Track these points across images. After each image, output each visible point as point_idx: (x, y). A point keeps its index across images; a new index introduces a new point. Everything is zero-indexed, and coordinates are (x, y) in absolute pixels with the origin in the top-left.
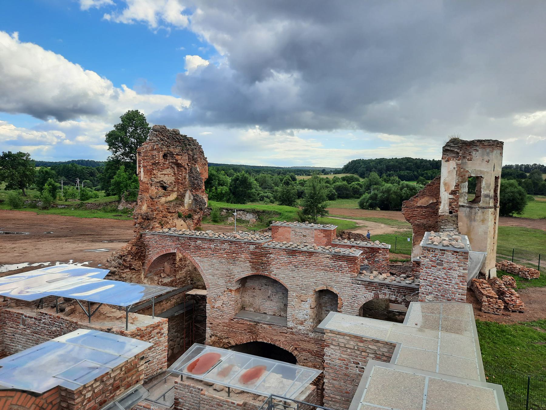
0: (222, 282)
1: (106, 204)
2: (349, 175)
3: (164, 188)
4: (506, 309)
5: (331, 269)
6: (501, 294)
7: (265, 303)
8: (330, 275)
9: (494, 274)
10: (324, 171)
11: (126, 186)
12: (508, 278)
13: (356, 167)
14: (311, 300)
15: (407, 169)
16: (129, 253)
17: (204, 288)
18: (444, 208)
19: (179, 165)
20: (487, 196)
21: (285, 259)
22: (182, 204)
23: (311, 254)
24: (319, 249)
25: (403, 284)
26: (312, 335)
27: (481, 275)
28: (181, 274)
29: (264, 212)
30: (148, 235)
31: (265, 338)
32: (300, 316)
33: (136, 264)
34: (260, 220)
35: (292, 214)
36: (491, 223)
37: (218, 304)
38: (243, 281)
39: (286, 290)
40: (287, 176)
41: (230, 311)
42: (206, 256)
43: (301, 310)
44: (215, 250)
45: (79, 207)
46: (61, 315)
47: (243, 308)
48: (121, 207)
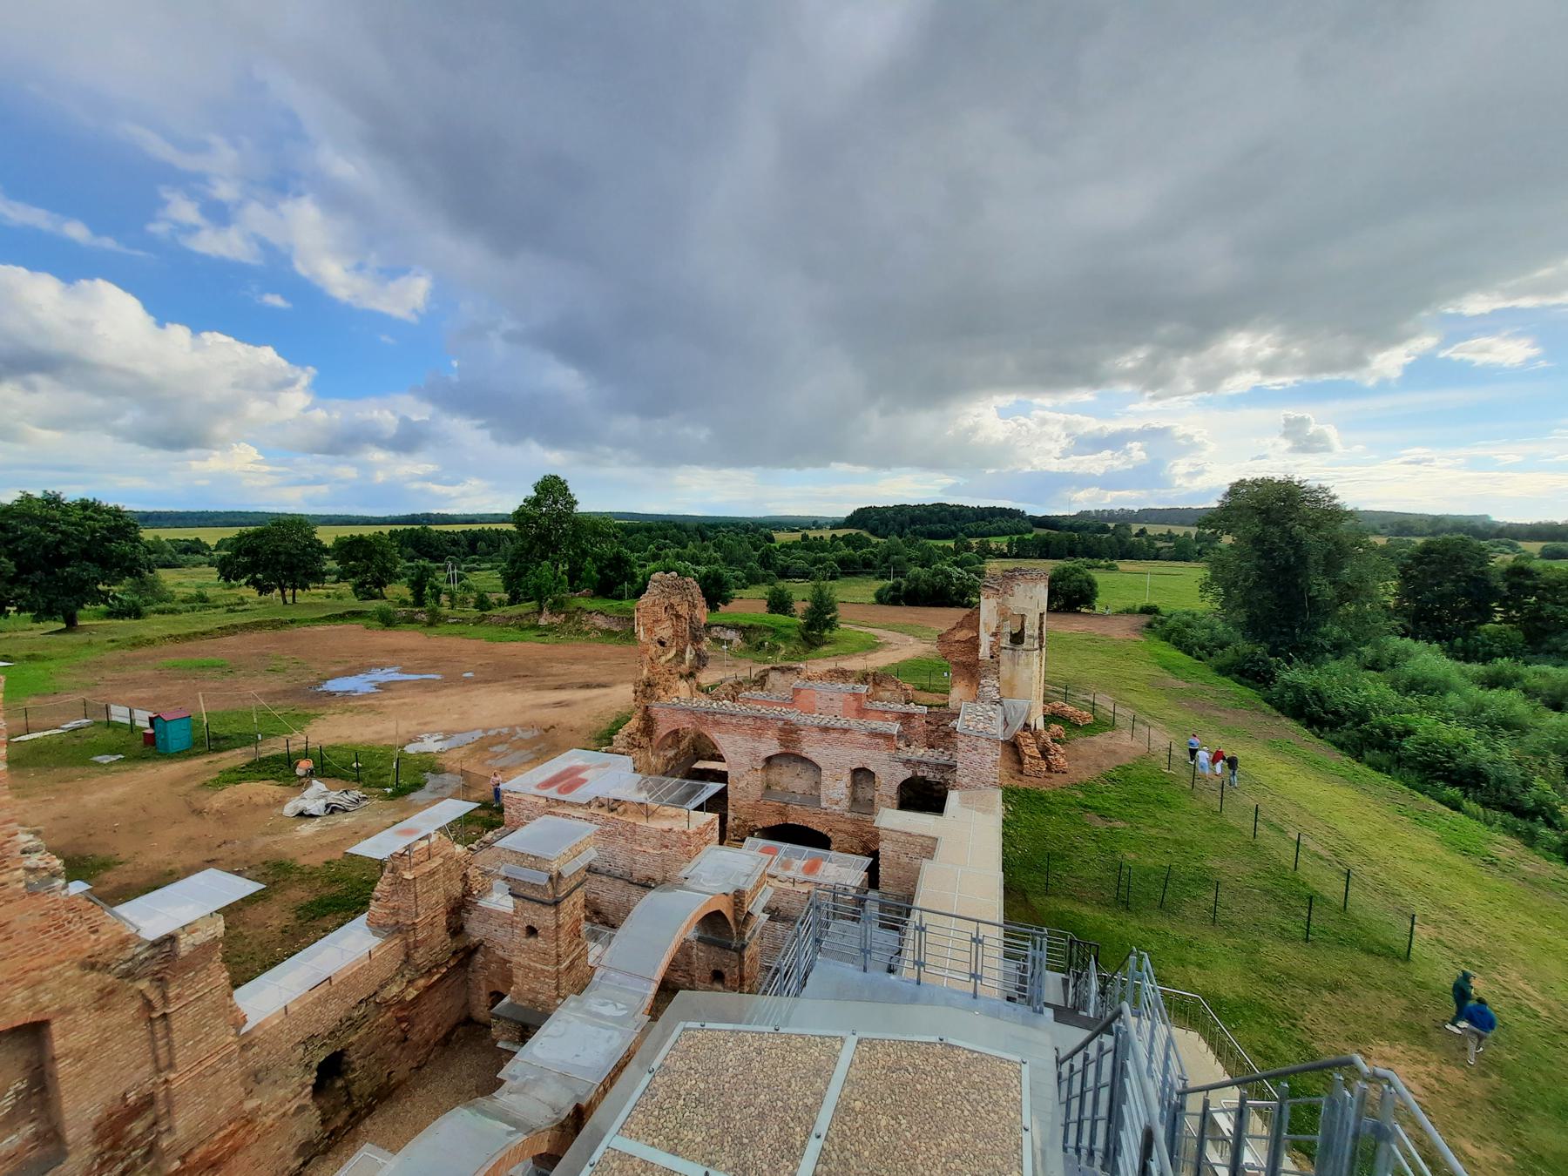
0: (745, 760)
1: (521, 617)
2: (854, 532)
3: (662, 644)
4: (1049, 769)
5: (868, 747)
6: (1044, 752)
7: (792, 780)
8: (867, 752)
9: (1040, 725)
10: (816, 524)
11: (549, 591)
12: (1055, 728)
13: (862, 518)
14: (847, 779)
15: (941, 521)
16: (638, 730)
17: (720, 758)
18: (984, 652)
19: (678, 616)
20: (1031, 637)
21: (817, 735)
22: (683, 661)
23: (846, 731)
24: (853, 723)
25: (941, 761)
26: (848, 815)
27: (1026, 726)
28: (684, 744)
29: (751, 626)
30: (655, 708)
31: (794, 819)
32: (836, 796)
33: (644, 741)
34: (746, 639)
35: (789, 631)
36: (1036, 668)
37: (742, 784)
38: (769, 760)
39: (818, 768)
40: (756, 532)
41: (756, 791)
42: (727, 732)
43: (836, 791)
44: (737, 726)
45: (479, 621)
46: (613, 815)
47: (768, 787)
48: (542, 622)
